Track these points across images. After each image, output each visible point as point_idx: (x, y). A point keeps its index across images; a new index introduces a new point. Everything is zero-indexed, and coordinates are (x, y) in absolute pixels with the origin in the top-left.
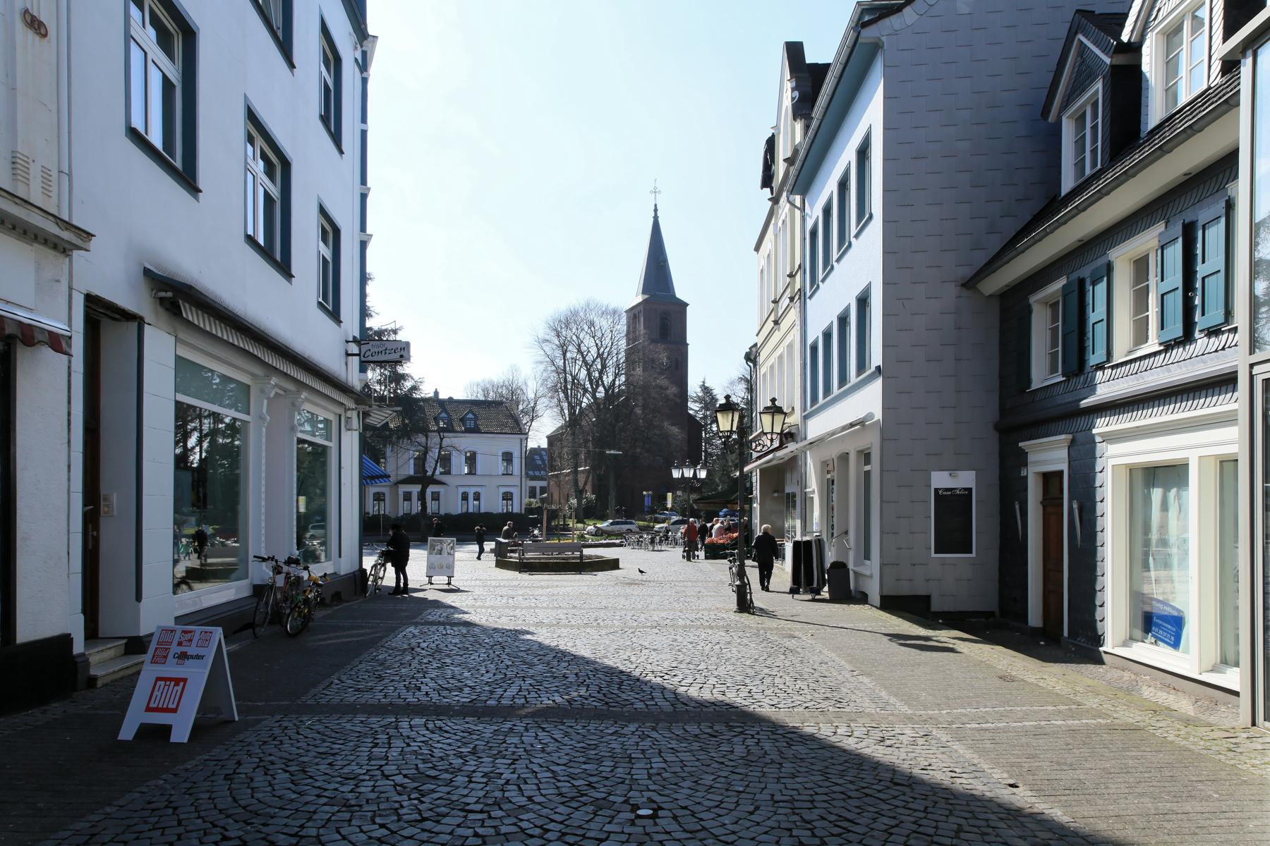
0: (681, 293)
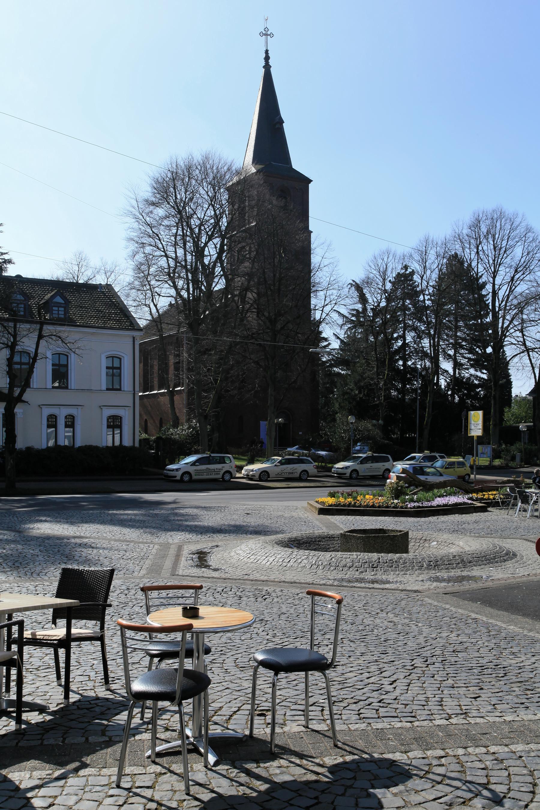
0: (299, 163)
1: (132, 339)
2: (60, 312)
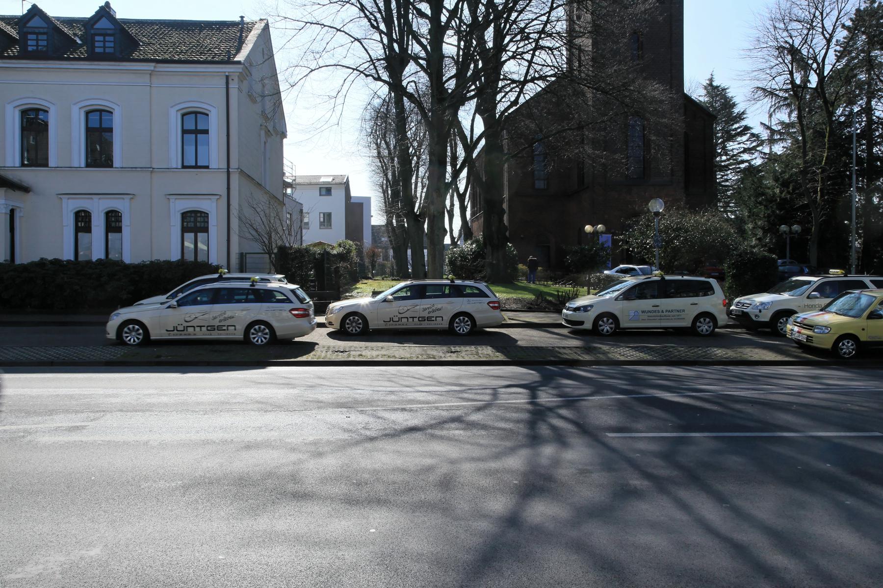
1: (224, 81)
2: (40, 43)
